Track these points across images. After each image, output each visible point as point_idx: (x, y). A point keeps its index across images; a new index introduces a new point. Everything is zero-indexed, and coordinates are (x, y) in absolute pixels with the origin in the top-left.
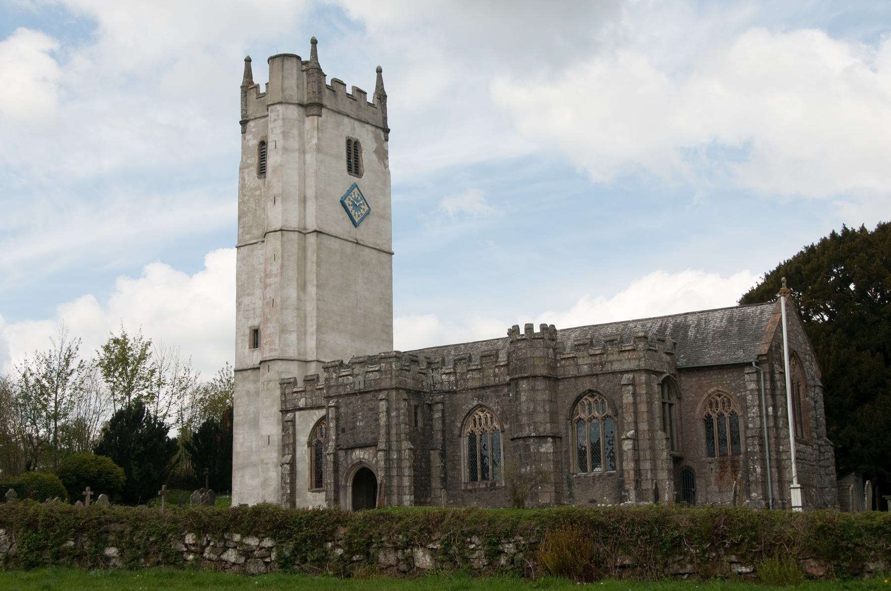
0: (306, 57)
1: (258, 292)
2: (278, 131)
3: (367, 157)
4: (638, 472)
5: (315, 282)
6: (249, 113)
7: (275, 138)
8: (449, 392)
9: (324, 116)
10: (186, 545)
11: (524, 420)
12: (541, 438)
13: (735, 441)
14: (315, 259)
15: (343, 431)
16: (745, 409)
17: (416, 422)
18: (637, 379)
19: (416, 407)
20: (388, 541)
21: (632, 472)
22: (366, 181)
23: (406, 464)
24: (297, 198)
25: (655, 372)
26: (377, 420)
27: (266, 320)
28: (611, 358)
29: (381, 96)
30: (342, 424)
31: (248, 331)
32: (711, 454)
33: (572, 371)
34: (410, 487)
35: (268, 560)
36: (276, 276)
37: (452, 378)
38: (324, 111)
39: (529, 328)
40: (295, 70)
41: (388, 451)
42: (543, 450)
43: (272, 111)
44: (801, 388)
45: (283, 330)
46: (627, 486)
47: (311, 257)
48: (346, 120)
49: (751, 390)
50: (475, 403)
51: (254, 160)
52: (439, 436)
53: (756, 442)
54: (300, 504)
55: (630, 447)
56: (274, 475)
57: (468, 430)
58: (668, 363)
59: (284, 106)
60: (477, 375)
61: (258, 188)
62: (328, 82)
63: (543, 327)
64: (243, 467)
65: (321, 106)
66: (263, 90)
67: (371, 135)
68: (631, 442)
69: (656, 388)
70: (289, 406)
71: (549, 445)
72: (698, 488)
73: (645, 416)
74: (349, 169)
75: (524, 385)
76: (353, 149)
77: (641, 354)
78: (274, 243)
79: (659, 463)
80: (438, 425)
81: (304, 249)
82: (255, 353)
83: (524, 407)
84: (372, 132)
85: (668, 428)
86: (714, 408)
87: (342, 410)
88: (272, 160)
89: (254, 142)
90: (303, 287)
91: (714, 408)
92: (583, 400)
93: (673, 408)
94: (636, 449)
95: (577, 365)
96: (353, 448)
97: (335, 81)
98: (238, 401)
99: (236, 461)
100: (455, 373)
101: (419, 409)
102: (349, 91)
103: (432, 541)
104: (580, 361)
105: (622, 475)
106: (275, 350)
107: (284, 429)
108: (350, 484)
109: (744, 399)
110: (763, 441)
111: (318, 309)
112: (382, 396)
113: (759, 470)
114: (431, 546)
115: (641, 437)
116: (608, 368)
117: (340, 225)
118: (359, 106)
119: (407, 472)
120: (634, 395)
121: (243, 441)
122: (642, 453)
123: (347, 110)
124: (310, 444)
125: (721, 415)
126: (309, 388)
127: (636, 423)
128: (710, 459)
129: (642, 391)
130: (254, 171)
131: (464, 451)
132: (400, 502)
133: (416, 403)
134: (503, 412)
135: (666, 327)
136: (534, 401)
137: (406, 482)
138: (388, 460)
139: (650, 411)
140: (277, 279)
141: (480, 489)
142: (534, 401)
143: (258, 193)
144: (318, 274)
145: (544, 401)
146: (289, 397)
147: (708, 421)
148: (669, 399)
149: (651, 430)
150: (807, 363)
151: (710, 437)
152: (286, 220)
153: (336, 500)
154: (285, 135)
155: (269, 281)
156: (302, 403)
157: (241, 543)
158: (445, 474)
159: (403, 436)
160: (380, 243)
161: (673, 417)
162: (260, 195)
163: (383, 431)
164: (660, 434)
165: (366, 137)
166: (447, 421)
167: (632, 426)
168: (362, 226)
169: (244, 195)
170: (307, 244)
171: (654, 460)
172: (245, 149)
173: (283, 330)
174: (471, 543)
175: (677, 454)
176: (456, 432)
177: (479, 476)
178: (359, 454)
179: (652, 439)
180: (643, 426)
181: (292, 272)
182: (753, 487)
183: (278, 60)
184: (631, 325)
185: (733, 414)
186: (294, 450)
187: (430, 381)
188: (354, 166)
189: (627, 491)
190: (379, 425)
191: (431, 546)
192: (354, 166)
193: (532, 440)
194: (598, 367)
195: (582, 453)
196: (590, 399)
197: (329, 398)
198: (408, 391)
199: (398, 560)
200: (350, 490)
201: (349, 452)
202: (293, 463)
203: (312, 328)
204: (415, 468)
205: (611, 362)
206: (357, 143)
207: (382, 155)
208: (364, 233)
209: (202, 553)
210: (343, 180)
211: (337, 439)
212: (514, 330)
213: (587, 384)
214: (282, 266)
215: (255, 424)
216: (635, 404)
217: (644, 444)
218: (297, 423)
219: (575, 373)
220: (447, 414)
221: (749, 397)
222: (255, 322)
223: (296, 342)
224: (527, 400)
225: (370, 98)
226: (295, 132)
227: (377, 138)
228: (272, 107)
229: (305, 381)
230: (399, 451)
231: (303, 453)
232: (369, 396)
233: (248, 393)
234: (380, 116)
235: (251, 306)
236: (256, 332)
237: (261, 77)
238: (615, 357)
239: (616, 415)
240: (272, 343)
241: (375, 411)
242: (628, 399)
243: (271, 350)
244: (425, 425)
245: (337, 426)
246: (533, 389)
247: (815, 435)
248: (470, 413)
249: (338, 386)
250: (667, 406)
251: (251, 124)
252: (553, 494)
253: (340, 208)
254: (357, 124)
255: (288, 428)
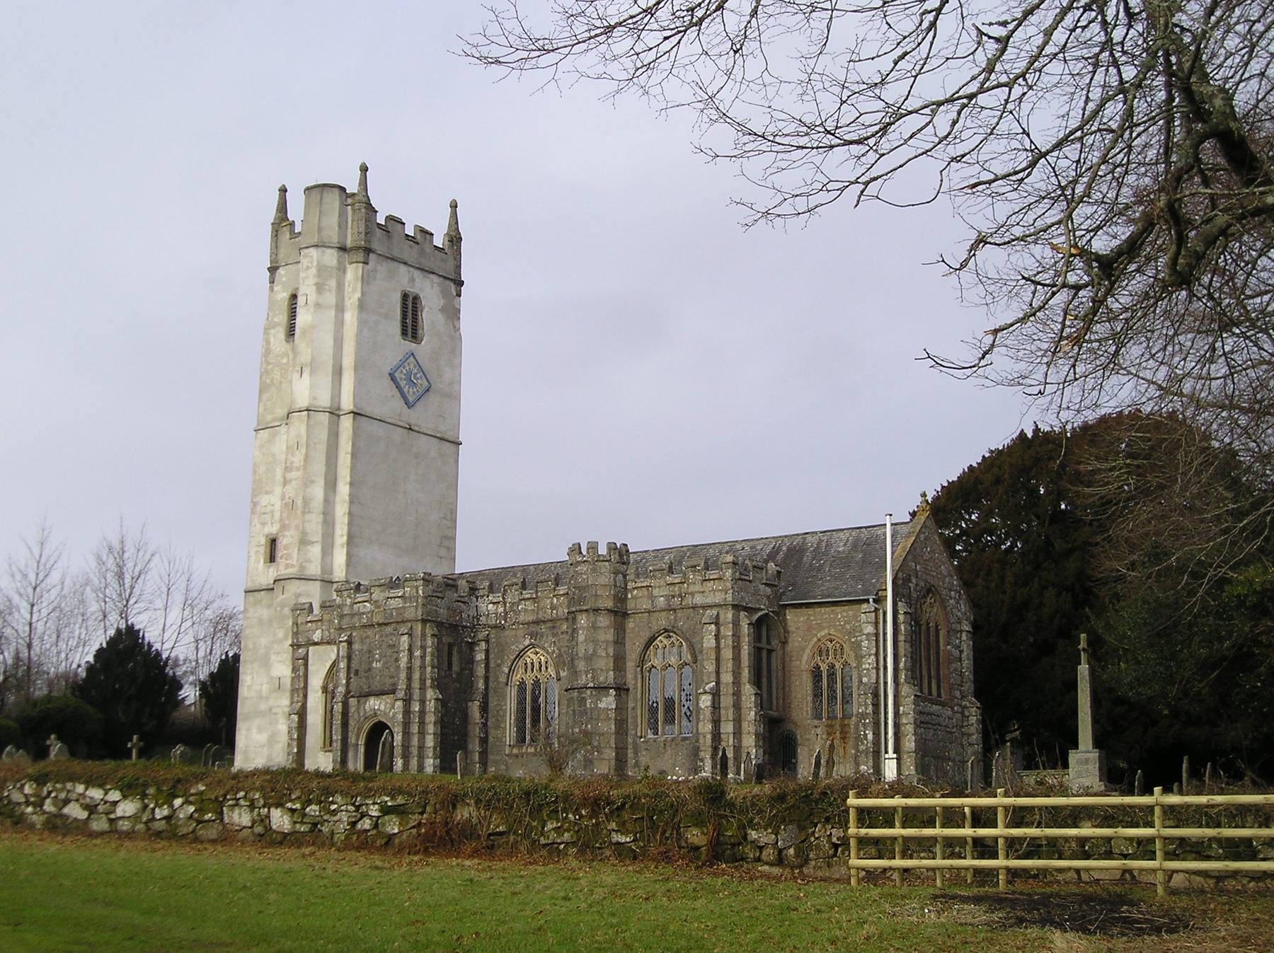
0: (352, 188)
1: (278, 490)
2: (312, 281)
3: (430, 316)
4: (716, 736)
5: (348, 479)
6: (281, 256)
7: (307, 292)
8: (495, 627)
9: (372, 264)
10: (26, 796)
11: (581, 665)
12: (601, 689)
13: (847, 700)
14: (349, 449)
15: (357, 673)
16: (859, 658)
17: (450, 665)
18: (722, 617)
19: (450, 646)
20: (245, 797)
21: (709, 736)
22: (424, 349)
23: (430, 719)
24: (330, 369)
25: (746, 609)
26: (397, 660)
27: (284, 527)
28: (692, 589)
29: (455, 239)
30: (354, 665)
31: (263, 541)
32: (818, 716)
33: (646, 605)
34: (435, 748)
35: (112, 816)
36: (298, 469)
37: (501, 609)
38: (372, 256)
39: (593, 547)
40: (337, 204)
41: (407, 701)
42: (602, 705)
43: (306, 256)
44: (942, 633)
45: (304, 542)
46: (702, 754)
47: (345, 446)
48: (403, 268)
49: (868, 635)
50: (527, 642)
51: (283, 318)
52: (481, 685)
53: (869, 701)
54: (310, 765)
55: (709, 703)
56: (283, 727)
57: (517, 678)
58: (768, 597)
59: (320, 250)
60: (530, 606)
61: (285, 354)
62: (381, 219)
63: (612, 547)
64: (247, 718)
65: (368, 251)
66: (298, 229)
67: (437, 288)
68: (709, 697)
69: (745, 628)
70: (302, 640)
71: (611, 699)
72: (800, 758)
73: (730, 665)
74: (404, 333)
75: (583, 620)
76: (410, 308)
77: (729, 585)
78: (299, 425)
79: (745, 725)
80: (480, 670)
81: (334, 435)
82: (271, 570)
83: (581, 650)
84: (439, 285)
85: (764, 680)
86: (824, 657)
87: (356, 647)
88: (302, 319)
89: (283, 296)
90: (331, 484)
91: (824, 657)
92: (657, 642)
93: (774, 655)
94: (716, 706)
95: (652, 598)
96: (368, 695)
97: (390, 218)
98: (248, 631)
99: (241, 709)
100: (505, 603)
101: (455, 649)
102: (410, 231)
103: (291, 801)
104: (656, 592)
105: (697, 741)
106: (293, 566)
107: (294, 669)
108: (362, 742)
109: (858, 646)
110: (878, 700)
111: (350, 514)
112: (404, 629)
113: (870, 737)
114: (289, 805)
115: (723, 690)
116: (689, 601)
117: (390, 406)
118: (422, 252)
119: (431, 729)
120: (717, 637)
121: (251, 685)
122: (723, 712)
123: (406, 257)
124: (325, 689)
125: (833, 666)
126: (326, 617)
127: (718, 673)
128: (816, 722)
129: (727, 632)
130: (280, 333)
131: (511, 705)
132: (421, 767)
133: (451, 640)
134: (560, 655)
135: (779, 549)
136: (595, 642)
137: (430, 742)
138: (407, 712)
139: (737, 658)
140: (300, 474)
141: (528, 754)
142: (595, 642)
143: (285, 361)
144: (353, 468)
145: (607, 642)
146: (301, 628)
147: (816, 674)
148: (769, 642)
149: (737, 682)
150: (952, 601)
151: (817, 695)
152: (315, 398)
153: (344, 761)
154: (320, 288)
155: (290, 476)
156: (317, 637)
157: (83, 795)
158: (487, 733)
159: (428, 682)
160: (443, 429)
161: (774, 666)
162: (288, 363)
163: (403, 675)
164: (748, 690)
165: (430, 293)
166: (492, 665)
167: (713, 677)
168: (419, 407)
169: (268, 363)
170: (341, 429)
171: (738, 721)
172: (272, 304)
173: (304, 542)
174: (332, 803)
175: (774, 714)
176: (503, 679)
177: (528, 737)
178: (373, 703)
179: (737, 694)
180: (727, 678)
181: (319, 467)
182: (862, 758)
183: (317, 191)
184: (738, 546)
185: (846, 664)
186: (305, 696)
187: (472, 613)
188: (411, 327)
189: (702, 760)
190: (398, 667)
191: (289, 805)
192: (411, 327)
193: (588, 692)
194: (677, 600)
195: (653, 711)
196: (665, 641)
197: (340, 629)
198: (439, 625)
199: (254, 822)
200: (362, 749)
201: (363, 700)
202: (302, 714)
203: (341, 537)
204: (442, 723)
205: (692, 594)
206: (416, 299)
207: (453, 313)
208: (422, 416)
209: (41, 806)
210: (394, 347)
211: (348, 683)
212: (576, 549)
213: (663, 621)
214: (307, 457)
215: (266, 663)
216: (718, 648)
217: (727, 701)
218: (310, 662)
219: (649, 607)
220: (492, 656)
221: (865, 643)
222: (273, 529)
223: (319, 556)
224: (586, 640)
225: (439, 241)
226: (333, 283)
227: (444, 293)
228: (306, 251)
229: (322, 607)
230: (423, 702)
231: (315, 701)
232: (389, 629)
233: (261, 621)
234: (451, 264)
235: (270, 508)
236: (273, 542)
237: (296, 212)
238: (698, 588)
239: (695, 661)
240: (288, 556)
241: (394, 647)
242: (709, 642)
243: (287, 566)
244: (462, 669)
245: (349, 667)
246: (594, 627)
247: (958, 694)
248: (519, 656)
249: (353, 615)
250: (764, 654)
251: (281, 271)
252: (613, 762)
253: (387, 382)
254: (417, 273)
255: (301, 666)
